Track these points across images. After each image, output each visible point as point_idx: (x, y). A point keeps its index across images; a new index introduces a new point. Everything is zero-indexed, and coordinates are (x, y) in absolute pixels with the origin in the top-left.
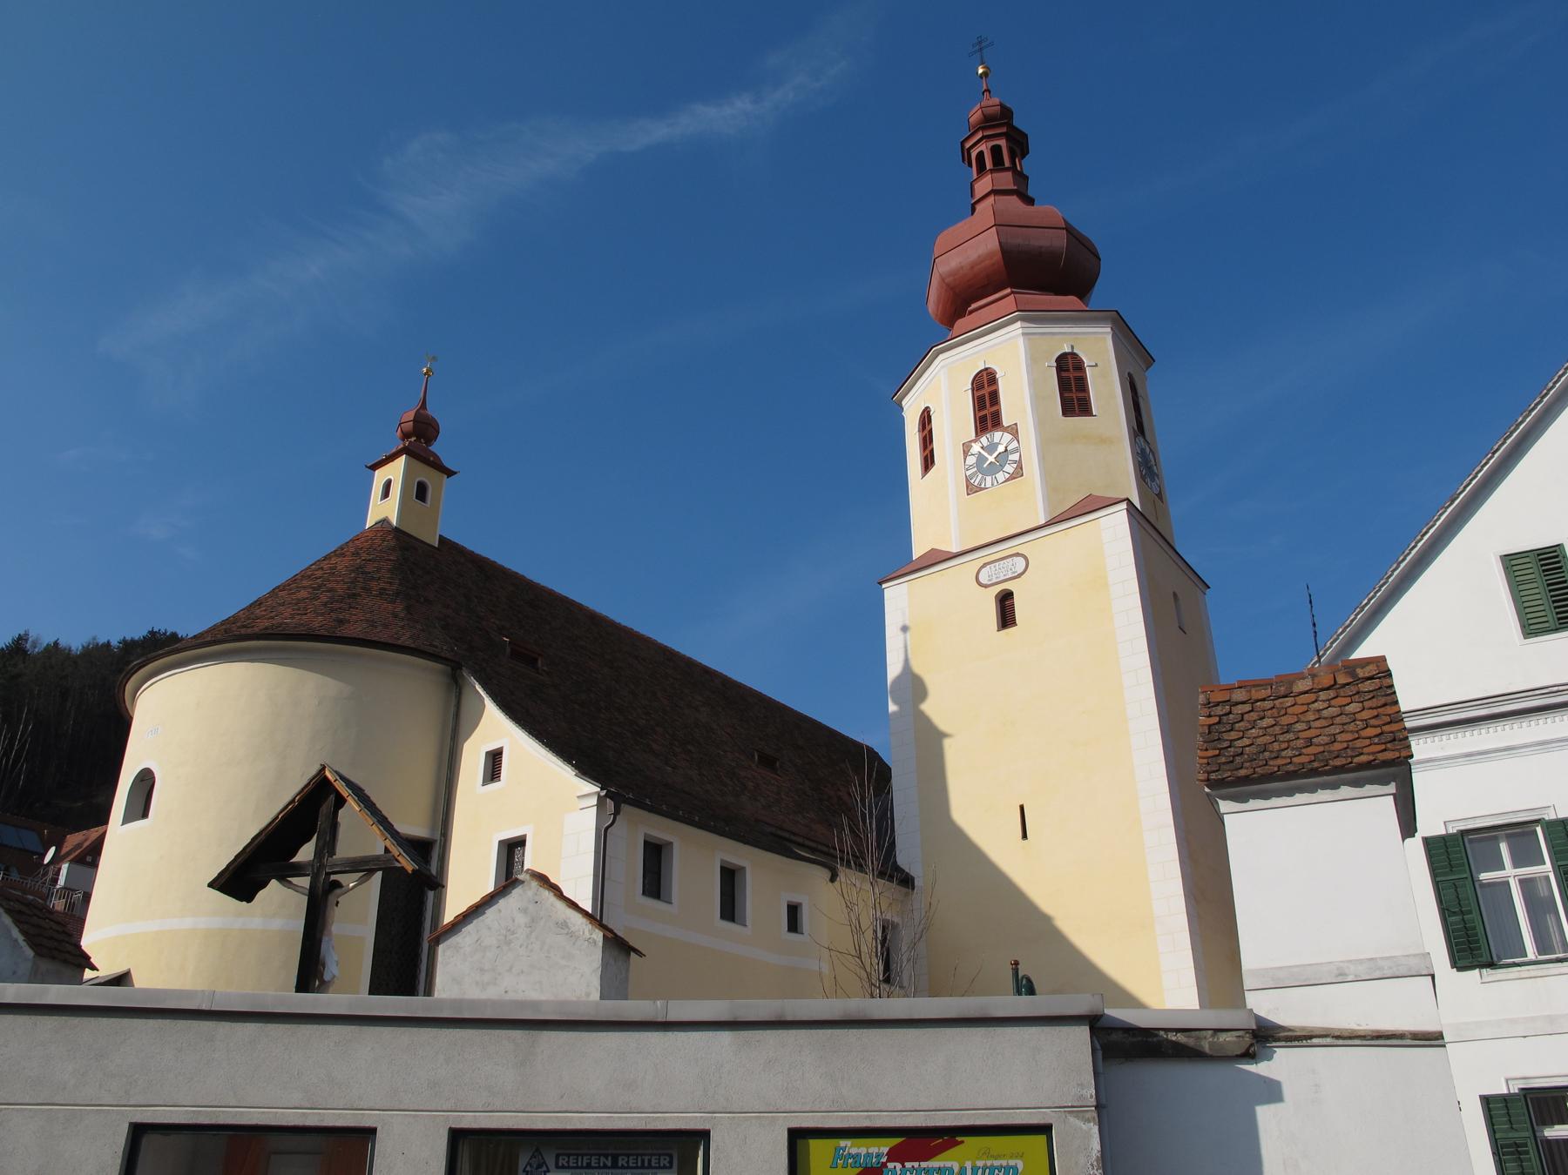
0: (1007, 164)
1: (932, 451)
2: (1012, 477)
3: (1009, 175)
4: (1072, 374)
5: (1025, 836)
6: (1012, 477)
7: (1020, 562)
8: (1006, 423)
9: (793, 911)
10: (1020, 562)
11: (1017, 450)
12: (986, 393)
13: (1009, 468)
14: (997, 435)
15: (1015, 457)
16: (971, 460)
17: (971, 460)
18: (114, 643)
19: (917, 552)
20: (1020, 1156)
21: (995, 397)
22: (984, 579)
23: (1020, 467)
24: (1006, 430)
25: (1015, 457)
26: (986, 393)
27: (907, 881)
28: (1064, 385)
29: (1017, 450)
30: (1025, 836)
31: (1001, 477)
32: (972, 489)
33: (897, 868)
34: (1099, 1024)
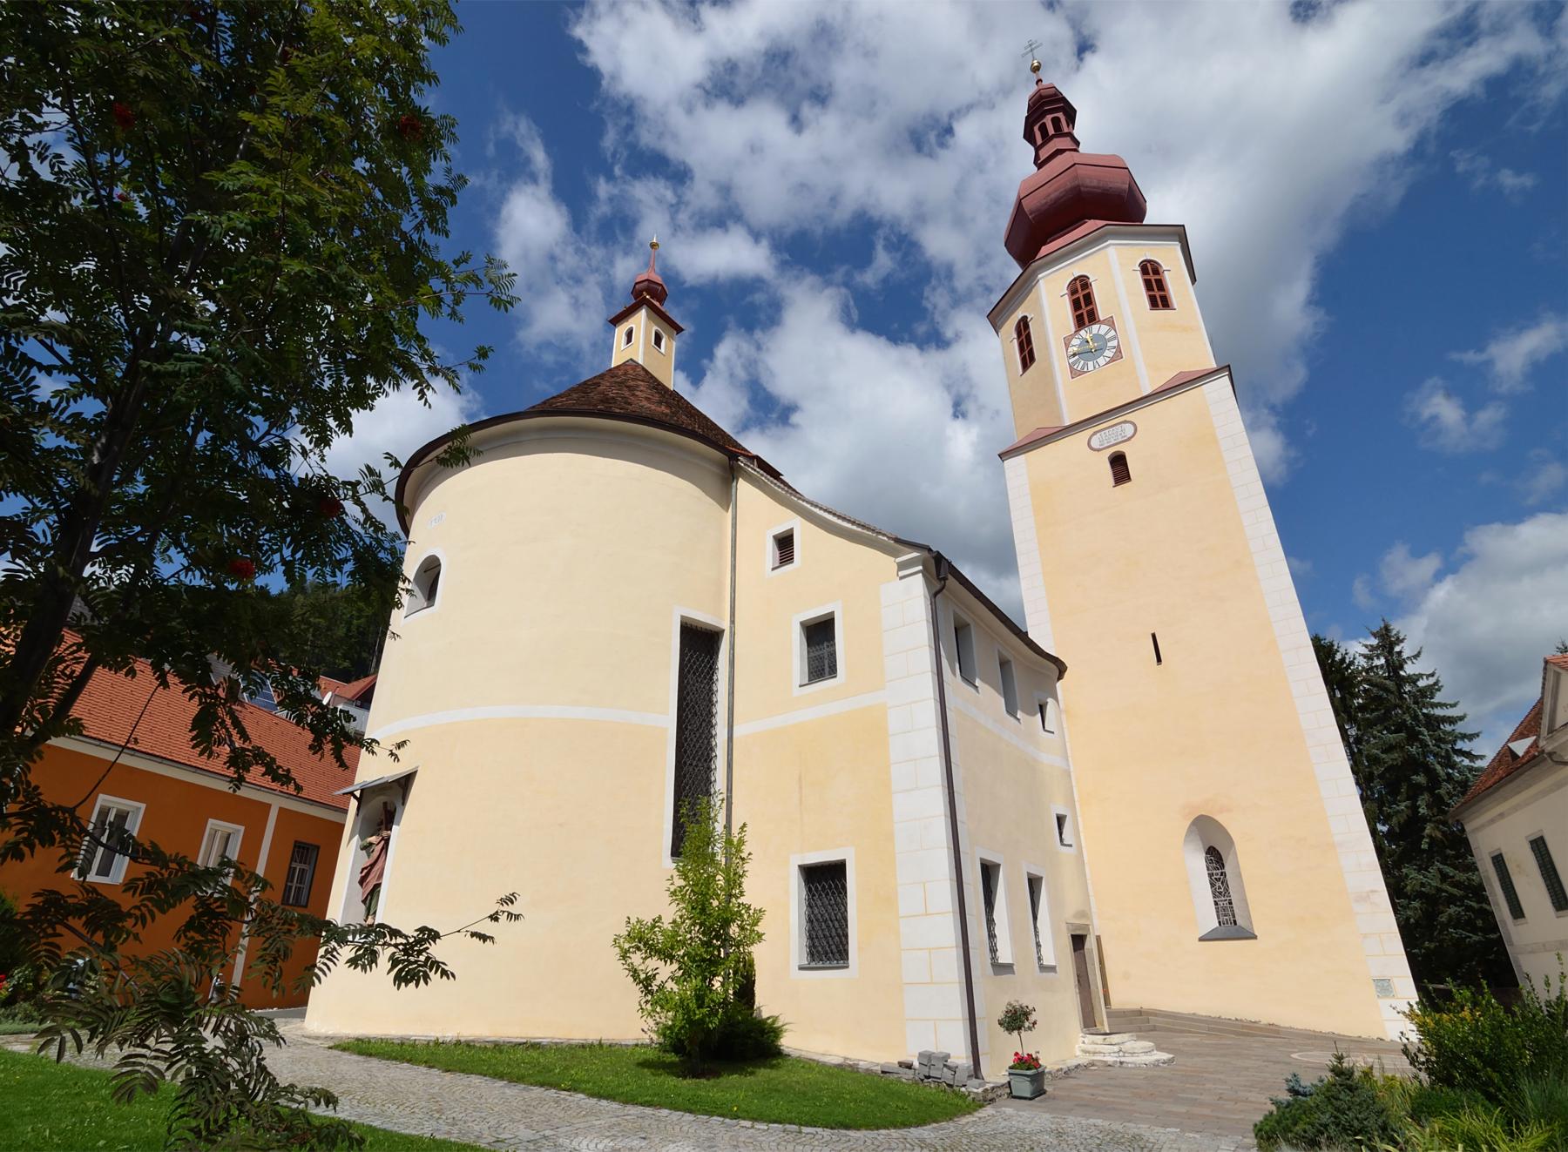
1: (1028, 337)
2: (1112, 360)
5: (1159, 660)
6: (1112, 360)
7: (1129, 429)
9: (820, 633)
11: (1115, 338)
12: (1083, 304)
13: (1109, 354)
14: (1095, 328)
15: (1114, 343)
20: (7, 308)
21: (1089, 299)
22: (1095, 444)
23: (1118, 350)
24: (1103, 322)
25: (1114, 343)
26: (1083, 304)
29: (1115, 338)
30: (1159, 660)
31: (1101, 361)
32: (1074, 373)
33: (753, 401)
34: (741, 83)
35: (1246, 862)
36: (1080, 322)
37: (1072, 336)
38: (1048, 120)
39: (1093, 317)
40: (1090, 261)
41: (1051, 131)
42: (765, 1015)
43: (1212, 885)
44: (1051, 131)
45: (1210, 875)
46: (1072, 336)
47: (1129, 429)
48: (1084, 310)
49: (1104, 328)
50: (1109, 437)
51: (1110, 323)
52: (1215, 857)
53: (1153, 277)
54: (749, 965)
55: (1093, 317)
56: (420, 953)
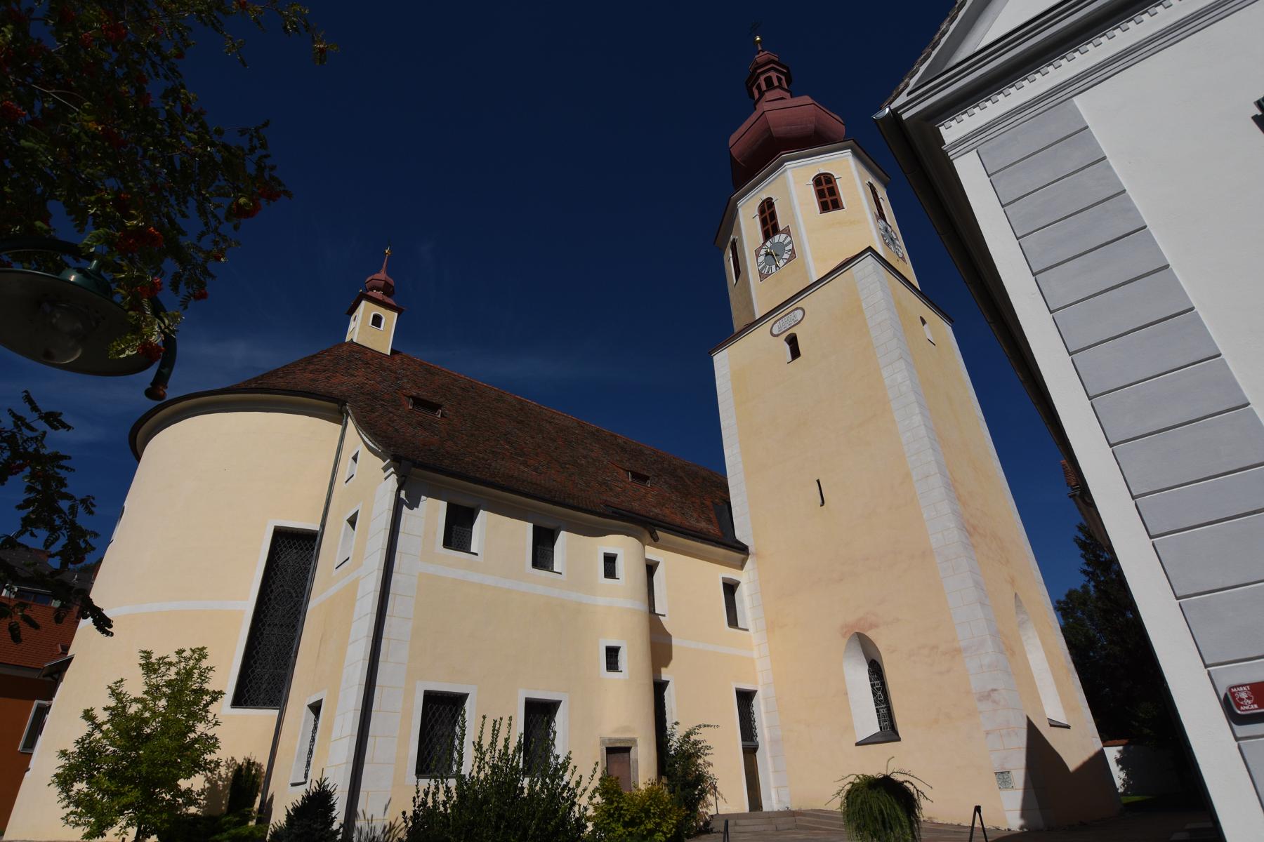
0: (776, 84)
2: (789, 260)
3: (778, 90)
4: (825, 187)
6: (789, 260)
7: (799, 313)
8: (781, 228)
10: (799, 313)
11: (790, 242)
13: (786, 256)
14: (776, 238)
15: (790, 247)
16: (761, 259)
17: (761, 259)
18: (1079, 589)
19: (736, 331)
21: (773, 216)
22: (775, 332)
23: (793, 251)
25: (790, 247)
27: (743, 549)
28: (820, 194)
31: (781, 263)
32: (763, 276)
35: (669, 694)
36: (767, 236)
37: (761, 248)
38: (762, 80)
39: (775, 230)
40: (772, 186)
41: (764, 87)
42: (300, 799)
43: (874, 694)
44: (764, 87)
45: (872, 686)
46: (761, 248)
47: (799, 314)
48: (769, 226)
49: (783, 236)
50: (781, 324)
51: (787, 231)
52: (876, 670)
53: (825, 187)
54: (423, 769)
55: (775, 230)
56: (136, 762)
